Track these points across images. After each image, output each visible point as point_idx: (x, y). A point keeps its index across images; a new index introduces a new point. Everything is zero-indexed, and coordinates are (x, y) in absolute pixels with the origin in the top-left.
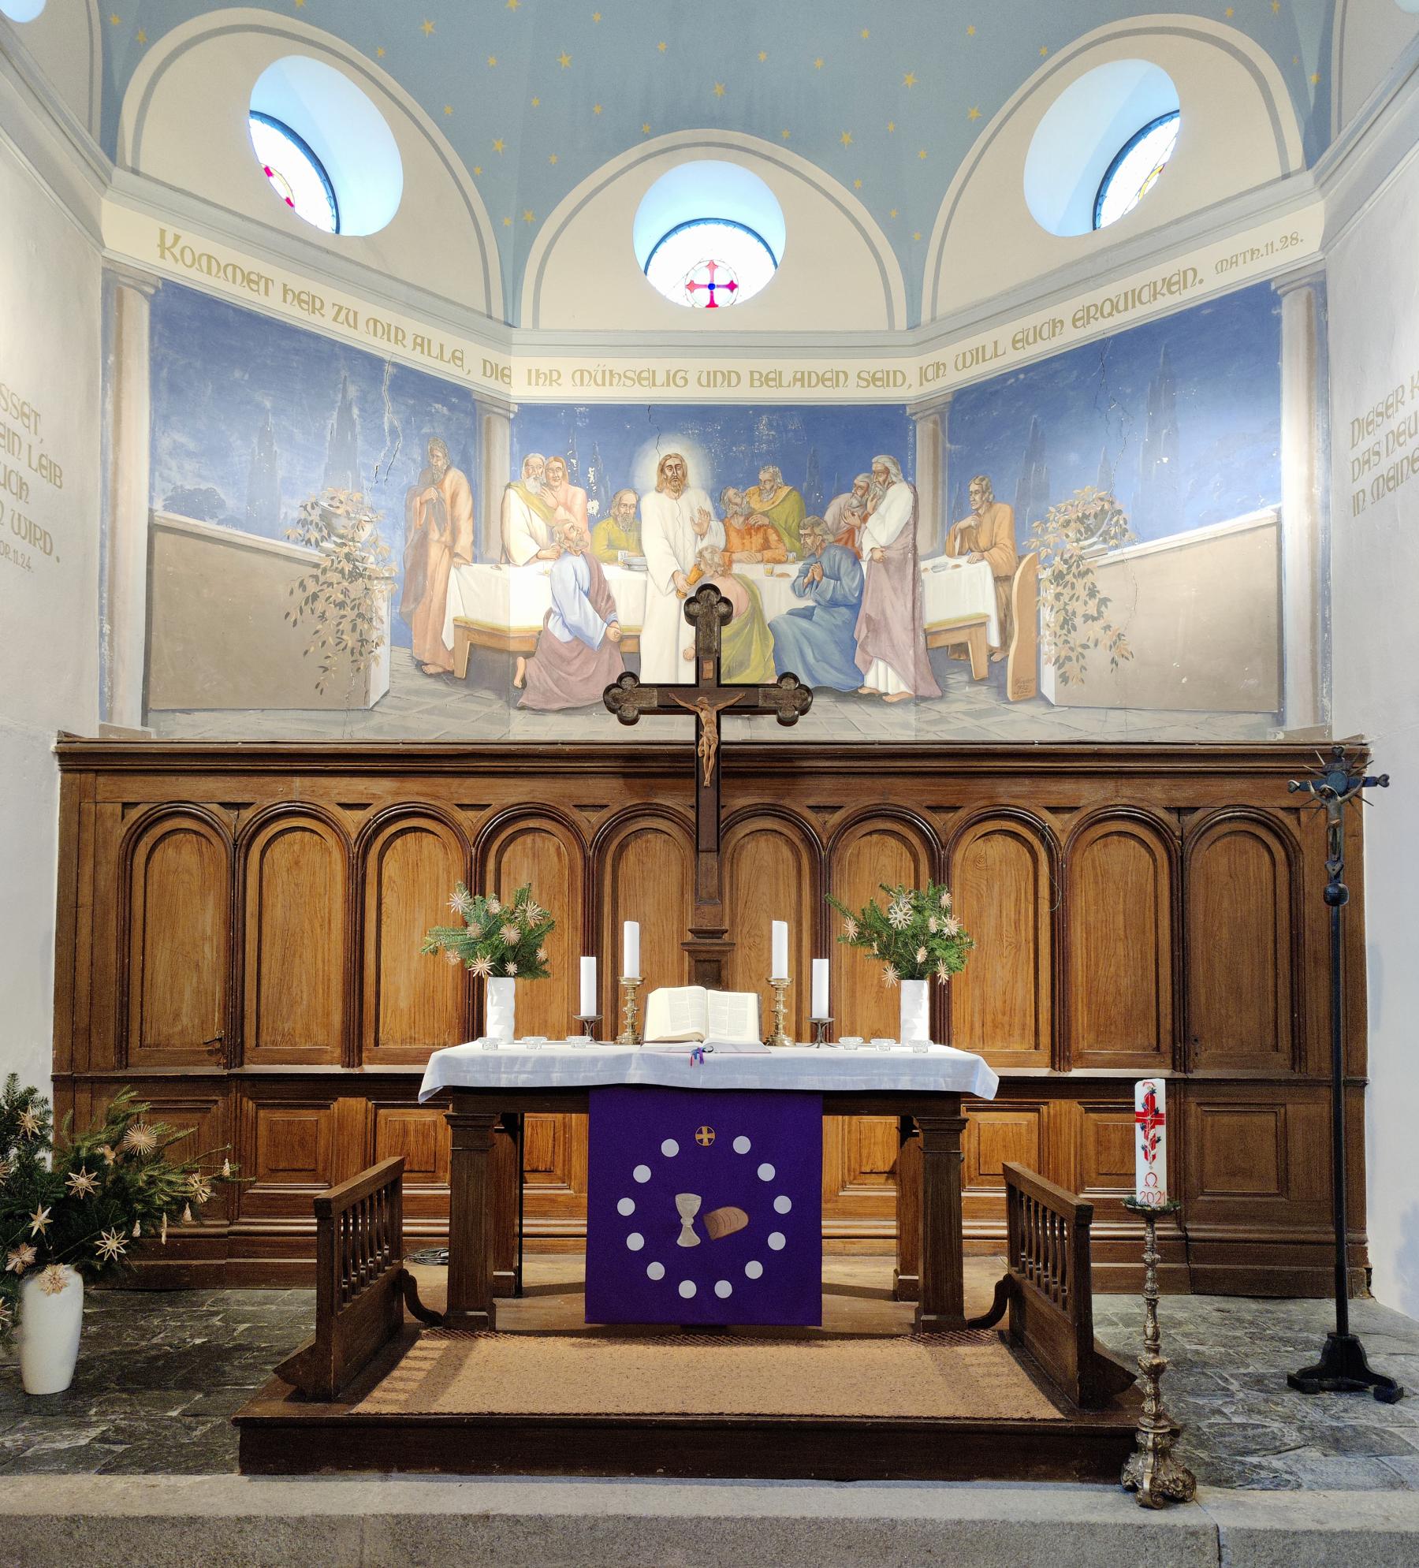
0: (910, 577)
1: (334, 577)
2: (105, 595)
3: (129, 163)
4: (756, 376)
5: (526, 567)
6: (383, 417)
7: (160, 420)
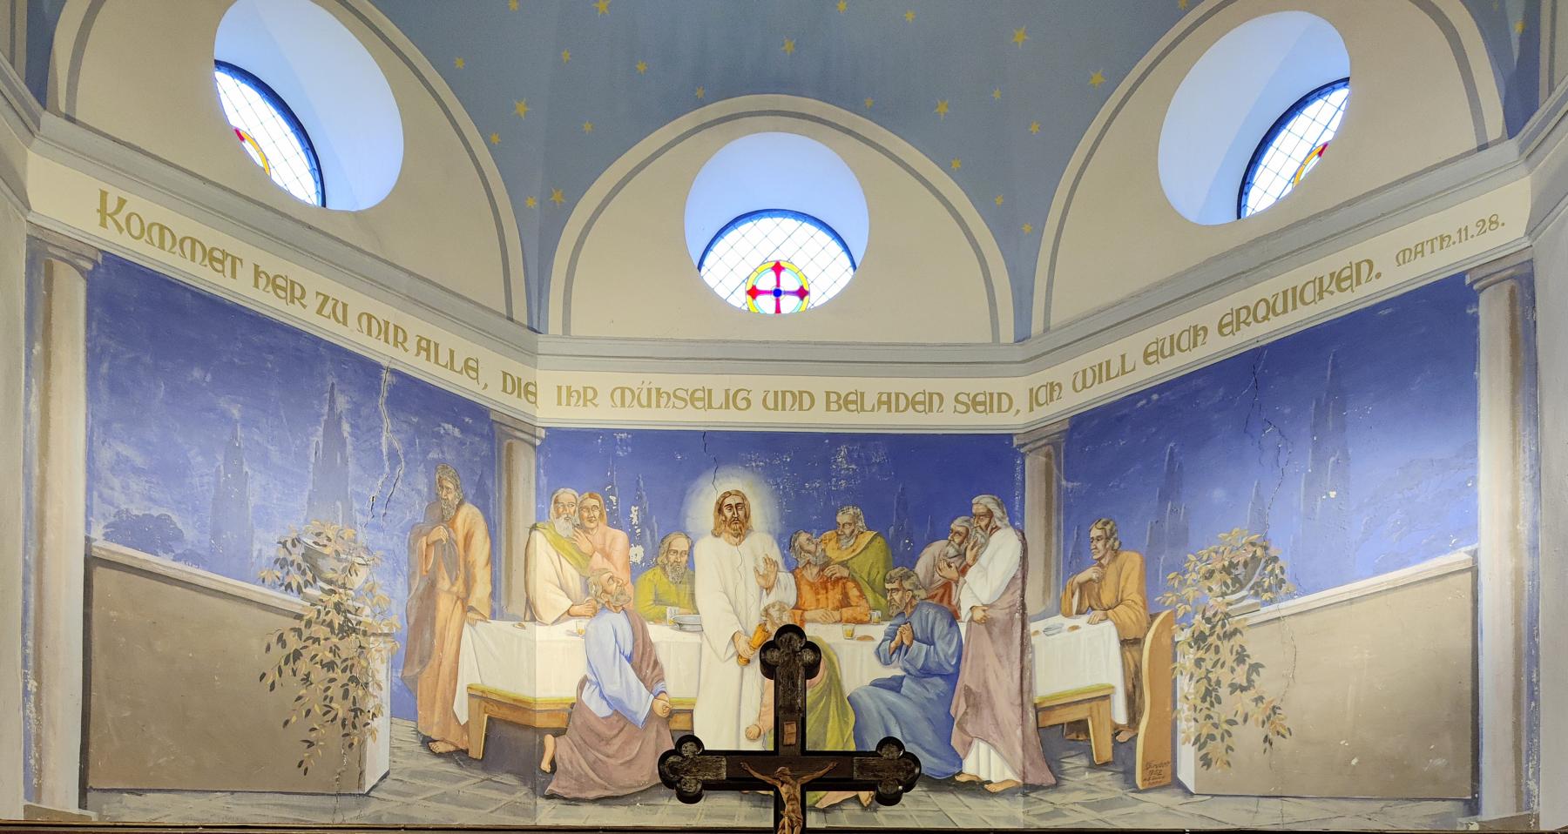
0: (1017, 641)
1: (320, 631)
2: (30, 643)
3: (63, 108)
4: (833, 398)
5: (552, 627)
6: (380, 437)
7: (98, 430)
